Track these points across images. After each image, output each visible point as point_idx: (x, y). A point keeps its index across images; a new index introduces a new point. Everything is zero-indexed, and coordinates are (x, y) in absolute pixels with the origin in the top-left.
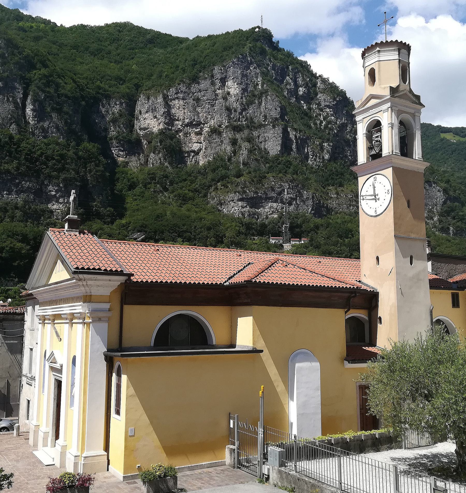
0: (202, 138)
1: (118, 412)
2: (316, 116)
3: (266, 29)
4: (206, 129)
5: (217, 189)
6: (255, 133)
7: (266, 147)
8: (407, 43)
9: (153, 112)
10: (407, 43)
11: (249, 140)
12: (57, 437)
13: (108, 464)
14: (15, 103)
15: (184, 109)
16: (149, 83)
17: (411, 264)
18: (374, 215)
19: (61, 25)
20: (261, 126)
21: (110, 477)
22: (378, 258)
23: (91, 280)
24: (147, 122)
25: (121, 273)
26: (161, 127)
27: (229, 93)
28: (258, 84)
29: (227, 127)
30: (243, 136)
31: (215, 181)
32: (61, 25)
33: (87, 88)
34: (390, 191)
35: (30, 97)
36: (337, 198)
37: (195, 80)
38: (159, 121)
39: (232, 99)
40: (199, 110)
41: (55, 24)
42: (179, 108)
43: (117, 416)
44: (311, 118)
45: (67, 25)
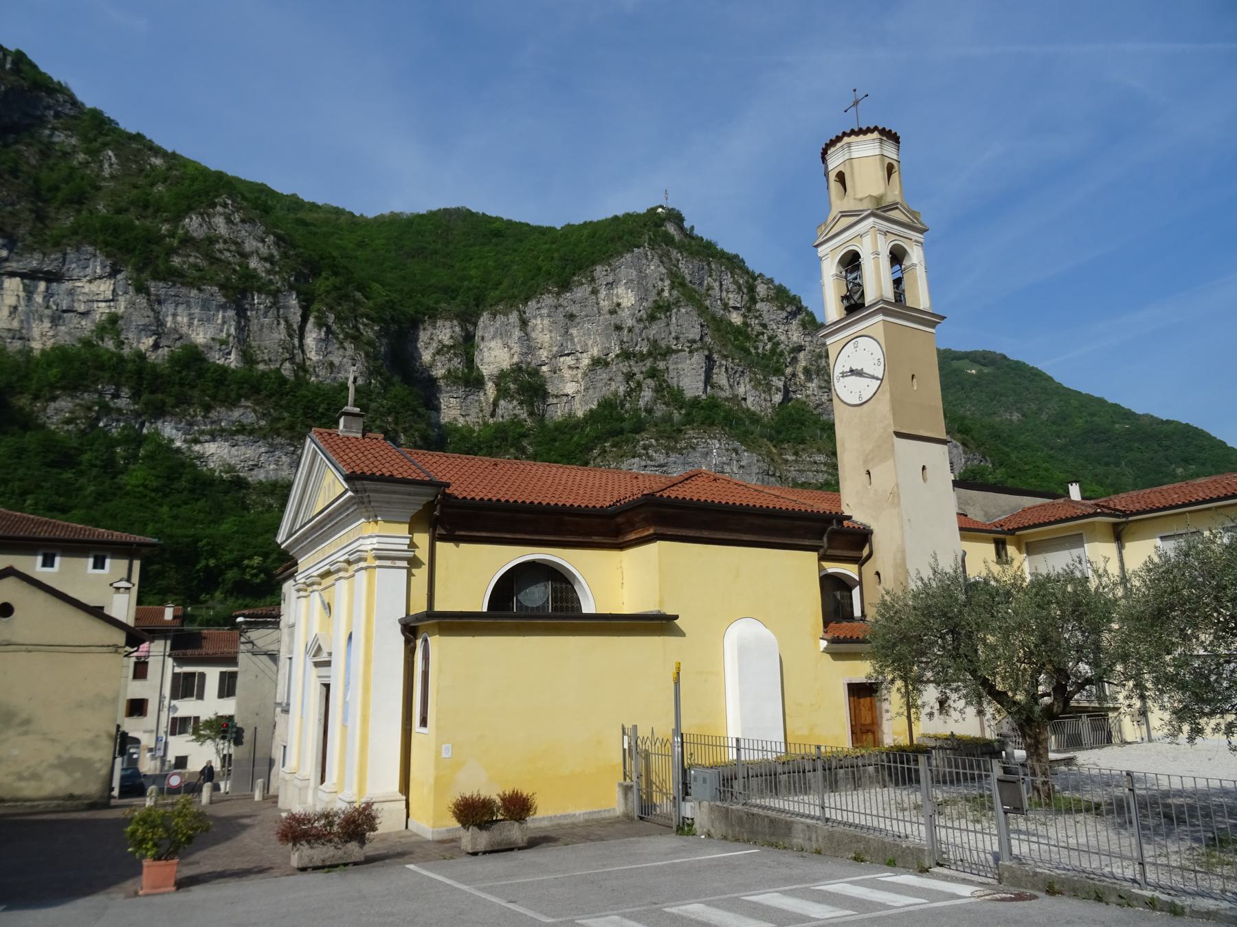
0: (580, 375)
1: (424, 722)
2: (757, 336)
3: (673, 209)
4: (586, 361)
5: (606, 452)
6: (661, 365)
7: (681, 384)
8: (893, 132)
9: (502, 338)
10: (893, 132)
11: (653, 373)
12: (323, 780)
13: (408, 816)
14: (289, 326)
15: (551, 331)
16: (495, 294)
17: (925, 480)
18: (859, 402)
19: (362, 215)
20: (669, 351)
21: (410, 836)
22: (869, 473)
23: (376, 491)
24: (493, 353)
25: (431, 484)
26: (516, 359)
27: (619, 305)
28: (663, 290)
29: (617, 356)
30: (644, 369)
31: (600, 438)
32: (362, 215)
33: (402, 305)
34: (882, 360)
35: (312, 320)
36: (796, 461)
37: (565, 286)
38: (512, 351)
39: (625, 314)
40: (574, 331)
41: (352, 214)
42: (543, 330)
43: (423, 730)
44: (748, 338)
45: (370, 214)
